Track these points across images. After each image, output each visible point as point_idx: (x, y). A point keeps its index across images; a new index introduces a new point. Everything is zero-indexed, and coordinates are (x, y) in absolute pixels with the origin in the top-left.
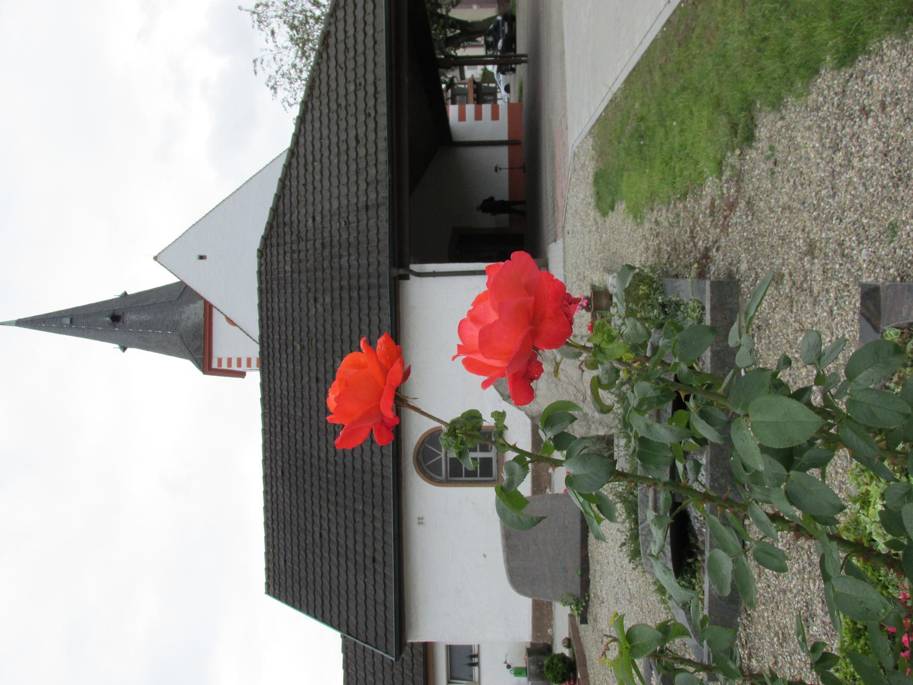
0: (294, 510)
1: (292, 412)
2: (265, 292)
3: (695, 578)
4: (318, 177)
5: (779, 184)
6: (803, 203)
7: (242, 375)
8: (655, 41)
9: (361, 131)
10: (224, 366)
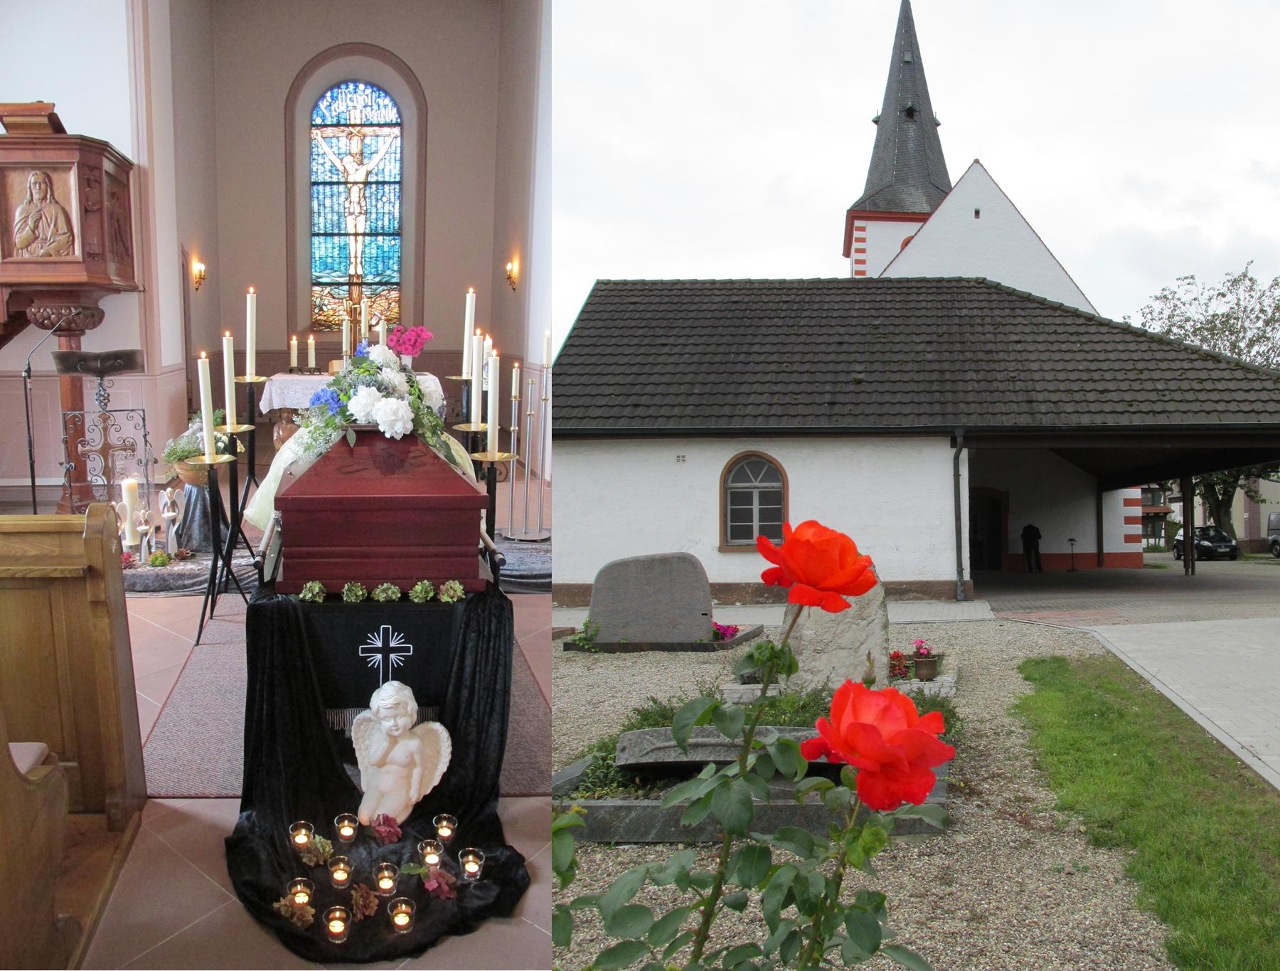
0: (693, 315)
1: (804, 314)
2: (939, 286)
3: (618, 787)
4: (1064, 347)
5: (1047, 878)
6: (1026, 908)
7: (847, 253)
8: (1203, 730)
9: (1114, 397)
10: (856, 234)
